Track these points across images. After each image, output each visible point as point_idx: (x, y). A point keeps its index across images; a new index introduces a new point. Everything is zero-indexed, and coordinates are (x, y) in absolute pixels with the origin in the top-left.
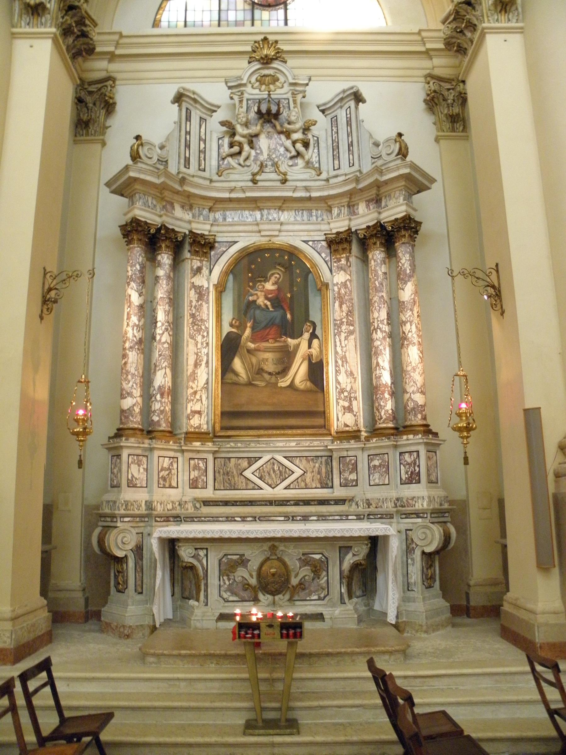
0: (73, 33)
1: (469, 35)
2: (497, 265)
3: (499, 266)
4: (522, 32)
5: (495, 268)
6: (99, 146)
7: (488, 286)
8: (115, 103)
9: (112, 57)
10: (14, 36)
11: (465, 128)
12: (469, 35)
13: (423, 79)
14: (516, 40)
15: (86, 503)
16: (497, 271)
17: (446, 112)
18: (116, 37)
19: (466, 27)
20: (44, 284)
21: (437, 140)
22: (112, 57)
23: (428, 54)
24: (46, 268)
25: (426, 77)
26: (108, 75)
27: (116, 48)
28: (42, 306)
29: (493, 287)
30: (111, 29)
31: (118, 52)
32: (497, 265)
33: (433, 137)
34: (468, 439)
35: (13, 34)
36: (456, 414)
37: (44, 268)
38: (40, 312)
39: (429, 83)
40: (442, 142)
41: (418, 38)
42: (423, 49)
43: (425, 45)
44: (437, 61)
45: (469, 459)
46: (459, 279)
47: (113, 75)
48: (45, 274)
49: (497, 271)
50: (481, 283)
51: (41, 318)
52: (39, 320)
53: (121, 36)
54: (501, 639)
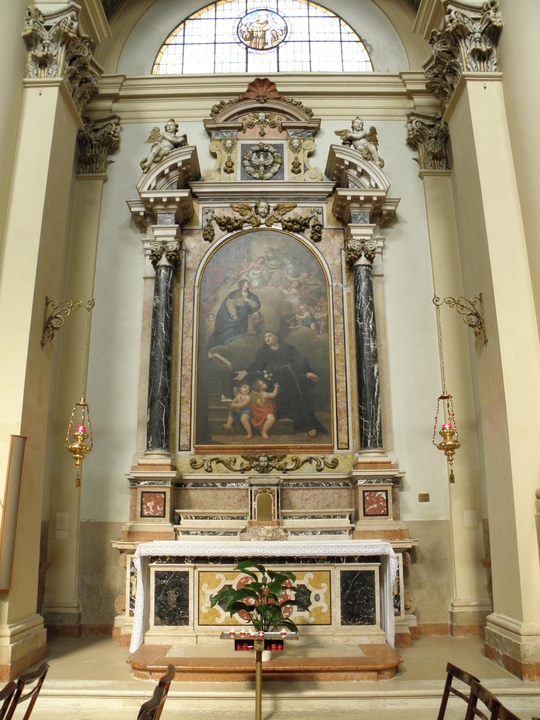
0: (86, 98)
1: (449, 79)
2: (481, 294)
3: (483, 296)
4: (500, 80)
5: (479, 298)
6: (101, 182)
7: (471, 314)
8: (118, 142)
9: (116, 98)
10: (25, 85)
11: (449, 166)
12: (449, 79)
13: (406, 118)
14: (495, 87)
15: (81, 520)
16: (481, 300)
17: (430, 149)
18: (120, 80)
19: (447, 73)
20: (45, 313)
21: (421, 176)
22: (116, 98)
23: (410, 95)
24: (49, 297)
25: (409, 116)
26: (112, 114)
27: (120, 90)
28: (44, 332)
29: (476, 315)
30: (116, 73)
31: (122, 93)
32: (481, 294)
33: (417, 174)
34: (453, 456)
35: (25, 83)
36: (440, 433)
37: (47, 298)
38: (41, 339)
39: (411, 123)
40: (425, 178)
41: (397, 79)
42: (404, 90)
43: (405, 87)
44: (418, 100)
45: (455, 477)
46: (444, 308)
47: (118, 114)
48: (47, 304)
49: (481, 300)
50: (465, 311)
51: (43, 345)
52: (40, 346)
53: (125, 79)
54: (400, 500)
